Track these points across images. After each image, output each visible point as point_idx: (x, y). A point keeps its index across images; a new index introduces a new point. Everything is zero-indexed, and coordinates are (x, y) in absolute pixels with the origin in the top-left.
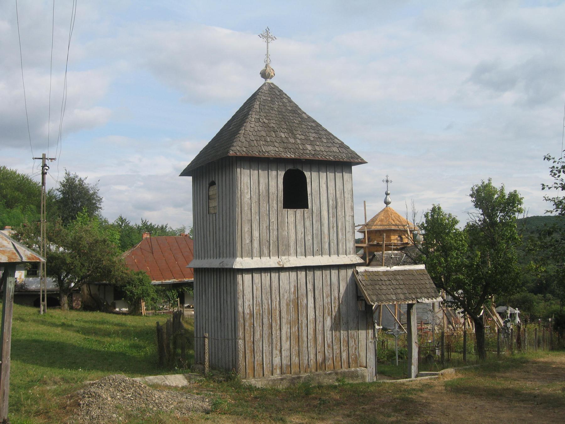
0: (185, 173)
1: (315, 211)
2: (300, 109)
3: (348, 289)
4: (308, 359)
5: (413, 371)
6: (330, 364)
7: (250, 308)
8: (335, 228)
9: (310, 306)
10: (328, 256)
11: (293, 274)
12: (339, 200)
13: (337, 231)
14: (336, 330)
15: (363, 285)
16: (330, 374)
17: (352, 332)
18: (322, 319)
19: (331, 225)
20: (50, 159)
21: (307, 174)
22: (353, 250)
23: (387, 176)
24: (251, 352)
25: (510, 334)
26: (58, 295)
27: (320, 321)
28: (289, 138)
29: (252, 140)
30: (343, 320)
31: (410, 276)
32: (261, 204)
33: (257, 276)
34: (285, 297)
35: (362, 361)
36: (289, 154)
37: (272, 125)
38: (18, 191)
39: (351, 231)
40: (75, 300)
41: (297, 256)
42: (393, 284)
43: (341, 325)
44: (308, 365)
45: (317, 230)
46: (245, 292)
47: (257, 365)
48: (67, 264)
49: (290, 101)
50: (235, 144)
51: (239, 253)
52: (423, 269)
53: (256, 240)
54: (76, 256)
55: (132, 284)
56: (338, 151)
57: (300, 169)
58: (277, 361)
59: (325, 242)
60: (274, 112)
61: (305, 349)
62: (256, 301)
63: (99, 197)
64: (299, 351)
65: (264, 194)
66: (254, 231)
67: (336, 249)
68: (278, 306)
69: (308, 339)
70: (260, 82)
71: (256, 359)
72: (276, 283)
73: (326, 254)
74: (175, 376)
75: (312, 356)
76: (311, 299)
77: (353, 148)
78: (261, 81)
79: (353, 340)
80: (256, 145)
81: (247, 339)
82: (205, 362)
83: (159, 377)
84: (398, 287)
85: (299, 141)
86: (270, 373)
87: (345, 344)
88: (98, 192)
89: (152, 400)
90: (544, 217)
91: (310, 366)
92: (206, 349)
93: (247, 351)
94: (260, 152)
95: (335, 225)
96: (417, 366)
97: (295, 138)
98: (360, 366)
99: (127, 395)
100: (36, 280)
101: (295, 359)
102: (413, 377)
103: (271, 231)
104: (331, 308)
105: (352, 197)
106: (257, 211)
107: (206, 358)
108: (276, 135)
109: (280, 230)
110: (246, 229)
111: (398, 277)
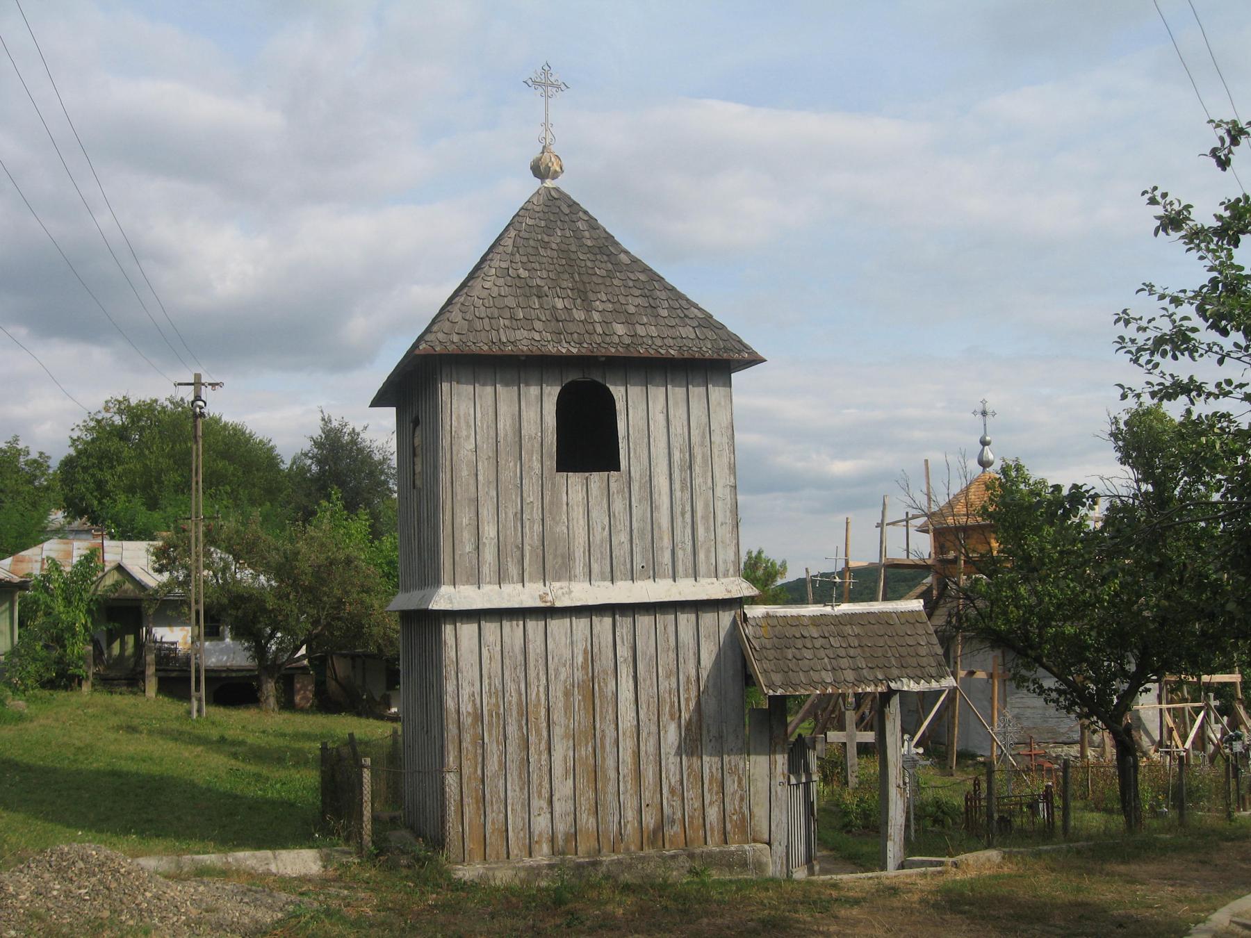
0: (379, 401)
1: (638, 477)
2: (616, 244)
3: (722, 659)
4: (620, 822)
5: (890, 854)
7: (474, 701)
8: (688, 515)
10: (670, 581)
11: (581, 624)
12: (697, 451)
14: (691, 754)
15: (755, 648)
16: (673, 857)
18: (654, 729)
19: (678, 509)
20: (210, 384)
21: (617, 391)
22: (734, 565)
24: (477, 803)
26: (257, 678)
27: (649, 734)
28: (575, 310)
29: (479, 318)
30: (709, 731)
31: (881, 627)
32: (502, 462)
33: (490, 628)
34: (562, 676)
35: (758, 828)
36: (566, 345)
39: (729, 521)
40: (299, 690)
41: (590, 581)
42: (832, 646)
43: (704, 742)
44: (621, 834)
47: (493, 832)
49: (593, 224)
51: (446, 574)
52: (917, 609)
53: (490, 544)
54: (289, 594)
56: (693, 336)
57: (600, 380)
58: (541, 823)
59: (662, 548)
62: (490, 685)
64: (596, 803)
65: (509, 439)
67: (690, 565)
69: (619, 773)
70: (525, 188)
71: (489, 819)
75: (630, 815)
76: (627, 682)
77: (732, 328)
79: (736, 778)
81: (466, 771)
82: (363, 822)
83: (261, 854)
85: (596, 316)
87: (715, 789)
92: (365, 792)
93: (465, 800)
94: (494, 343)
95: (688, 508)
97: (588, 310)
98: (755, 841)
99: (79, 888)
100: (217, 645)
102: (891, 872)
103: (527, 524)
104: (679, 702)
106: (492, 478)
107: (365, 813)
109: (548, 522)
110: (465, 521)
111: (848, 630)
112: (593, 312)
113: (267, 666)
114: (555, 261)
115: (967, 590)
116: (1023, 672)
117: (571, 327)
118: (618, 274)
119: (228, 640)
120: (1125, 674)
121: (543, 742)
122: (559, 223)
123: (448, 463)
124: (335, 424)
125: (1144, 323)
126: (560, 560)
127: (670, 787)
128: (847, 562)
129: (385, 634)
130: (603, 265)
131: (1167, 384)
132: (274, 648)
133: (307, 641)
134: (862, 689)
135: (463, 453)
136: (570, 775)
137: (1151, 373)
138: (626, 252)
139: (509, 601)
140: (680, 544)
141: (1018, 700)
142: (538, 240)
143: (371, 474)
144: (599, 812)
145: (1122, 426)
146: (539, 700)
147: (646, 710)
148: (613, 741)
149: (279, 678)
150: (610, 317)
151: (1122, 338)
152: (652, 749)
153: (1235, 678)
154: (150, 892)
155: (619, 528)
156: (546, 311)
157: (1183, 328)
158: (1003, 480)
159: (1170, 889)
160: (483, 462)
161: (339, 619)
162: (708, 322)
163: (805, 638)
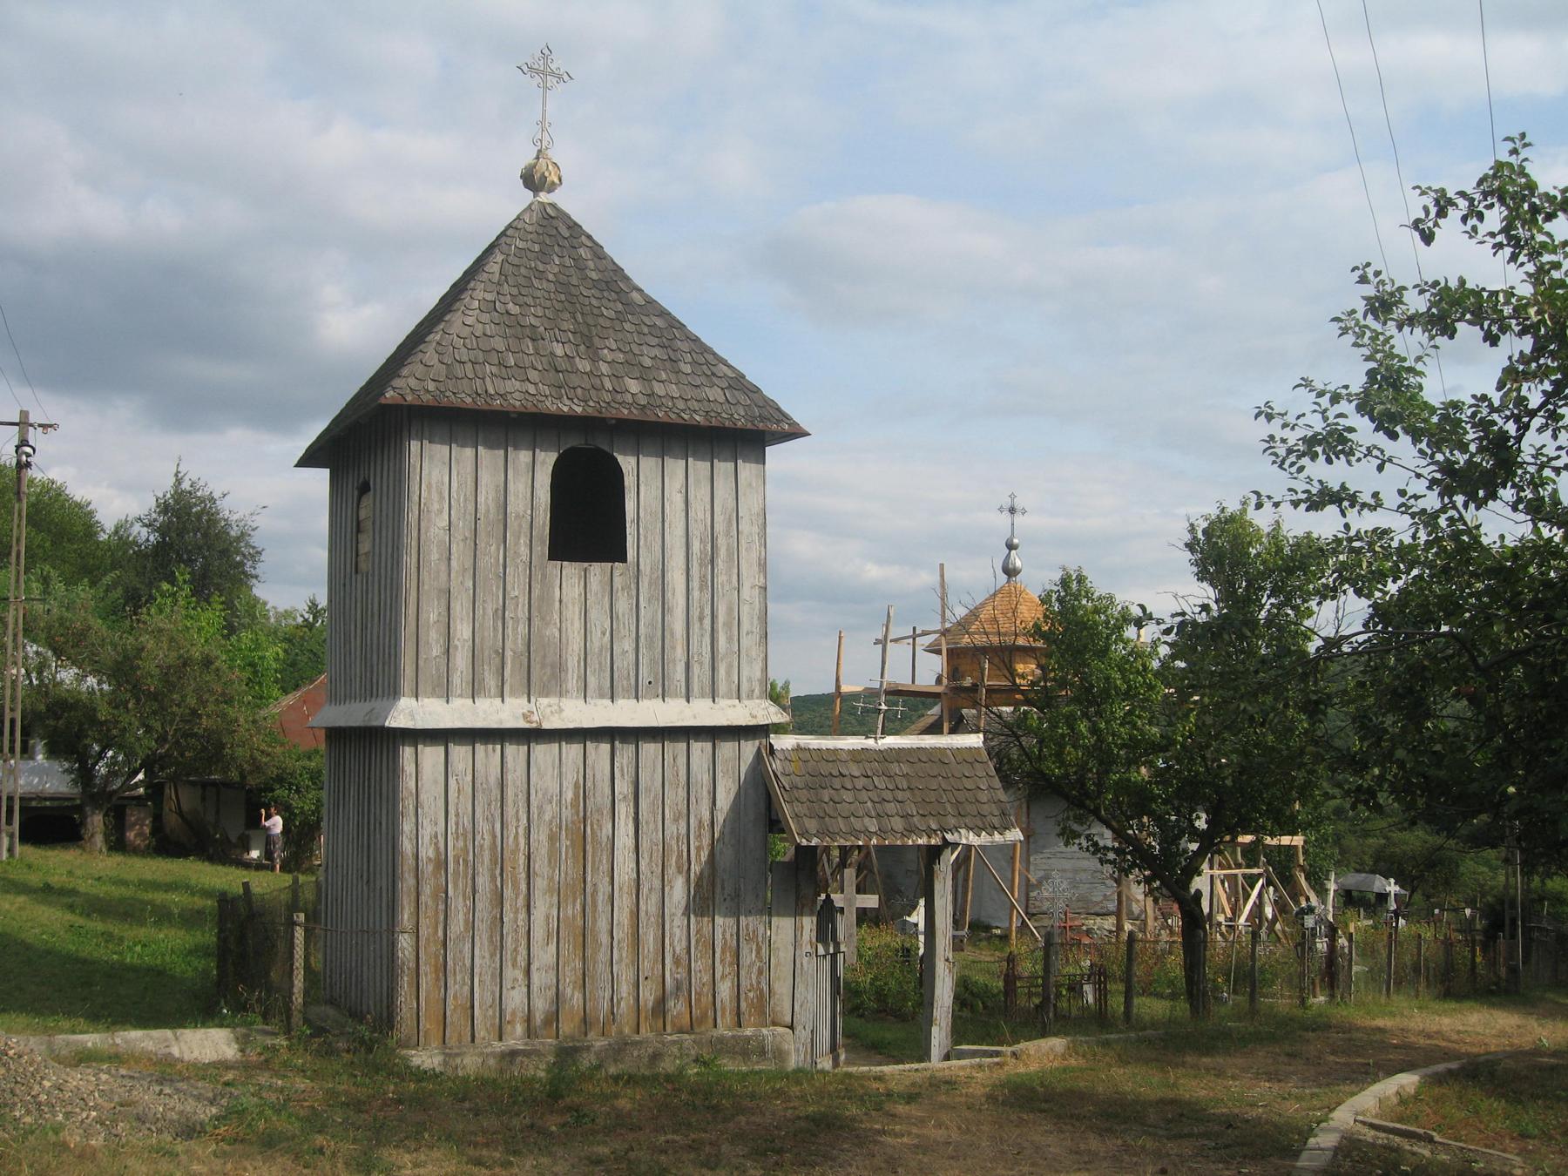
0: (309, 460)
1: (648, 572)
2: (627, 279)
3: (742, 799)
5: (935, 1042)
6: (678, 1014)
7: (436, 844)
8: (707, 621)
9: (621, 846)
10: (683, 701)
11: (573, 751)
12: (722, 542)
13: (713, 628)
14: (701, 913)
15: (784, 788)
17: (749, 922)
18: (657, 883)
19: (695, 613)
20: (40, 425)
21: (627, 463)
23: (1012, 496)
26: (79, 809)
27: (650, 890)
30: (723, 888)
32: (481, 545)
33: (460, 752)
35: (778, 1009)
36: (568, 402)
39: (756, 630)
40: (135, 824)
41: (585, 698)
44: (613, 1013)
45: (652, 625)
46: (422, 797)
47: (454, 1010)
48: (102, 724)
49: (597, 251)
50: (405, 372)
51: (407, 683)
53: (463, 647)
54: (127, 702)
55: (291, 784)
56: (722, 399)
57: (606, 448)
58: (515, 999)
62: (457, 824)
63: (254, 548)
65: (491, 516)
66: (455, 623)
68: (522, 841)
69: (612, 938)
70: (513, 202)
71: (451, 992)
72: (518, 773)
74: (206, 1033)
75: (625, 989)
76: (626, 824)
79: (754, 947)
81: (423, 932)
83: (156, 1033)
85: (604, 368)
87: (728, 959)
88: (252, 533)
89: (29, 1094)
92: (296, 956)
93: (422, 968)
94: (479, 395)
95: (708, 611)
96: (949, 1029)
97: (595, 358)
98: (774, 1024)
101: (574, 998)
102: (935, 1062)
103: (510, 623)
104: (689, 851)
105: (761, 534)
106: (469, 563)
107: (296, 982)
109: (536, 622)
110: (433, 617)
111: (895, 768)
112: (601, 362)
113: (93, 793)
114: (552, 296)
115: (1013, 724)
116: (1076, 827)
117: (574, 380)
118: (630, 316)
119: (40, 757)
120: (1195, 834)
121: (521, 897)
122: (556, 248)
123: (414, 543)
124: (186, 486)
125: (1291, 419)
126: (548, 671)
127: (674, 955)
128: (838, 687)
129: (251, 756)
130: (611, 305)
131: (1314, 491)
132: (103, 771)
133: (148, 765)
134: (913, 841)
135: (434, 531)
136: (552, 939)
137: (1295, 478)
138: (640, 290)
139: (484, 719)
140: (696, 657)
141: (1044, 861)
142: (531, 268)
143: (225, 553)
144: (587, 985)
145: (1200, 535)
146: (517, 845)
147: (648, 860)
148: (606, 897)
149: (109, 809)
150: (620, 370)
151: (1272, 437)
152: (654, 909)
153: (1298, 840)
154: (49, 1080)
155: (623, 633)
156: (543, 359)
157: (1340, 428)
158: (1063, 594)
159: (1267, 1084)
160: (458, 544)
161: (194, 735)
162: (739, 383)
163: (844, 776)
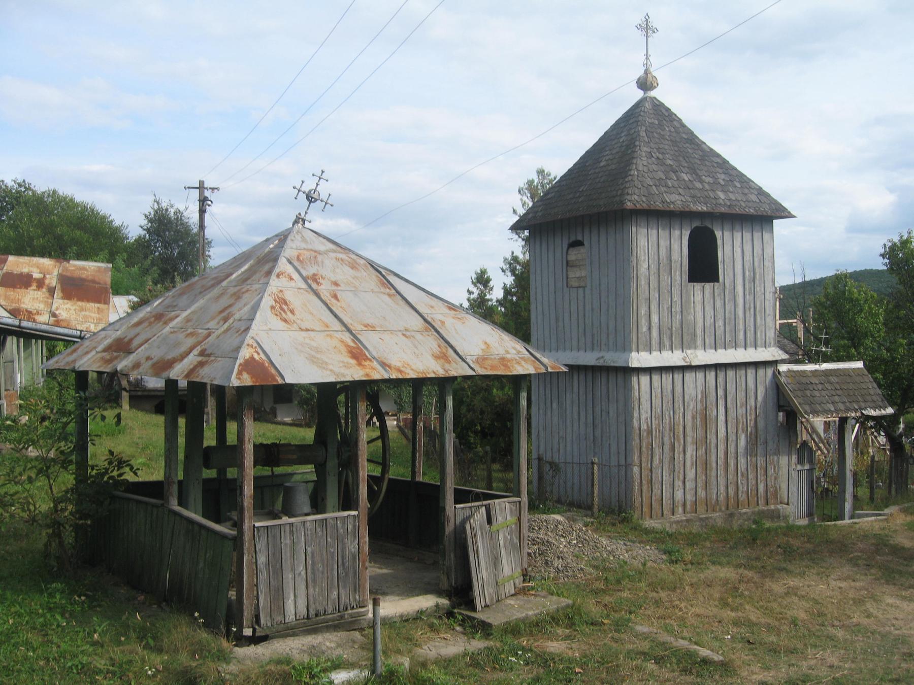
4: (717, 493)
8: (752, 310)
11: (700, 375)
12: (757, 270)
18: (734, 438)
19: (747, 306)
20: (210, 188)
21: (718, 234)
25: (23, 442)
27: (732, 440)
32: (661, 276)
33: (656, 378)
36: (699, 205)
37: (669, 162)
38: (78, 229)
43: (758, 445)
45: (730, 312)
46: (642, 400)
51: (634, 347)
56: (758, 201)
57: (710, 226)
58: (679, 495)
60: (667, 142)
61: (713, 479)
73: (740, 347)
75: (722, 489)
78: (640, 94)
80: (657, 193)
81: (643, 465)
84: (834, 394)
85: (707, 187)
86: (670, 513)
87: (762, 473)
90: (881, 270)
91: (719, 502)
95: (752, 305)
97: (701, 181)
98: (781, 503)
101: (701, 493)
103: (674, 314)
108: (677, 177)
110: (643, 312)
111: (832, 379)
